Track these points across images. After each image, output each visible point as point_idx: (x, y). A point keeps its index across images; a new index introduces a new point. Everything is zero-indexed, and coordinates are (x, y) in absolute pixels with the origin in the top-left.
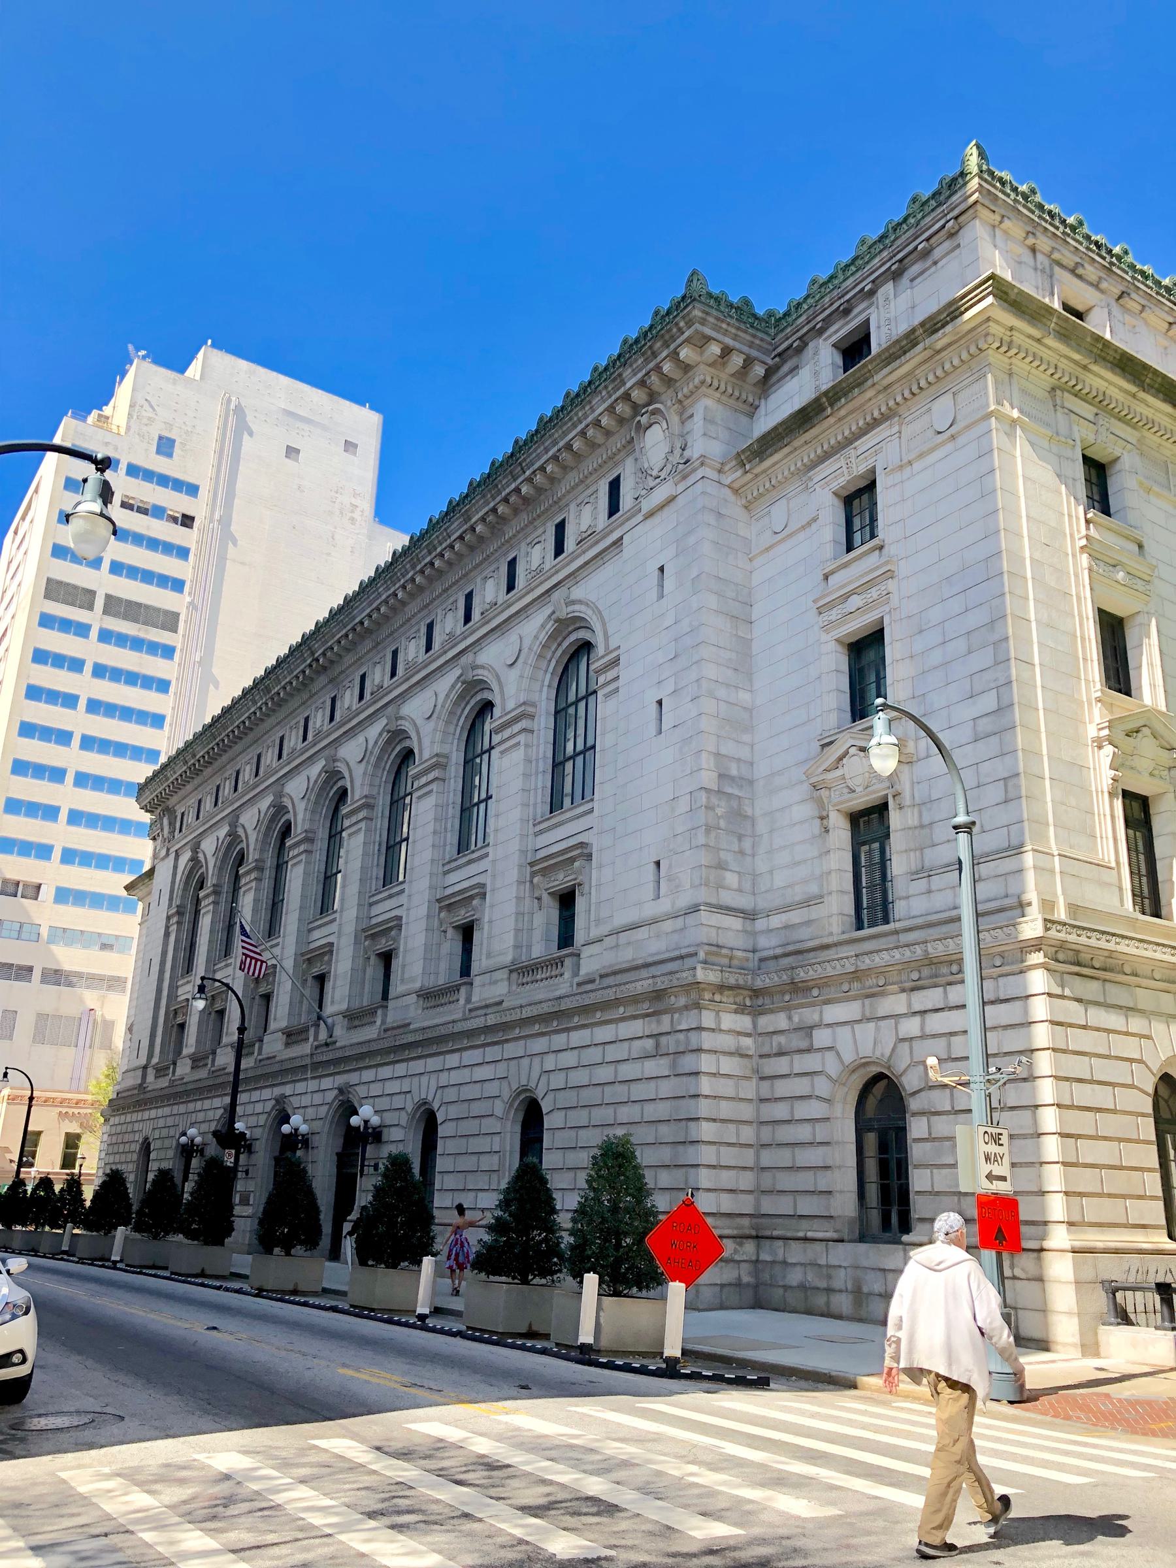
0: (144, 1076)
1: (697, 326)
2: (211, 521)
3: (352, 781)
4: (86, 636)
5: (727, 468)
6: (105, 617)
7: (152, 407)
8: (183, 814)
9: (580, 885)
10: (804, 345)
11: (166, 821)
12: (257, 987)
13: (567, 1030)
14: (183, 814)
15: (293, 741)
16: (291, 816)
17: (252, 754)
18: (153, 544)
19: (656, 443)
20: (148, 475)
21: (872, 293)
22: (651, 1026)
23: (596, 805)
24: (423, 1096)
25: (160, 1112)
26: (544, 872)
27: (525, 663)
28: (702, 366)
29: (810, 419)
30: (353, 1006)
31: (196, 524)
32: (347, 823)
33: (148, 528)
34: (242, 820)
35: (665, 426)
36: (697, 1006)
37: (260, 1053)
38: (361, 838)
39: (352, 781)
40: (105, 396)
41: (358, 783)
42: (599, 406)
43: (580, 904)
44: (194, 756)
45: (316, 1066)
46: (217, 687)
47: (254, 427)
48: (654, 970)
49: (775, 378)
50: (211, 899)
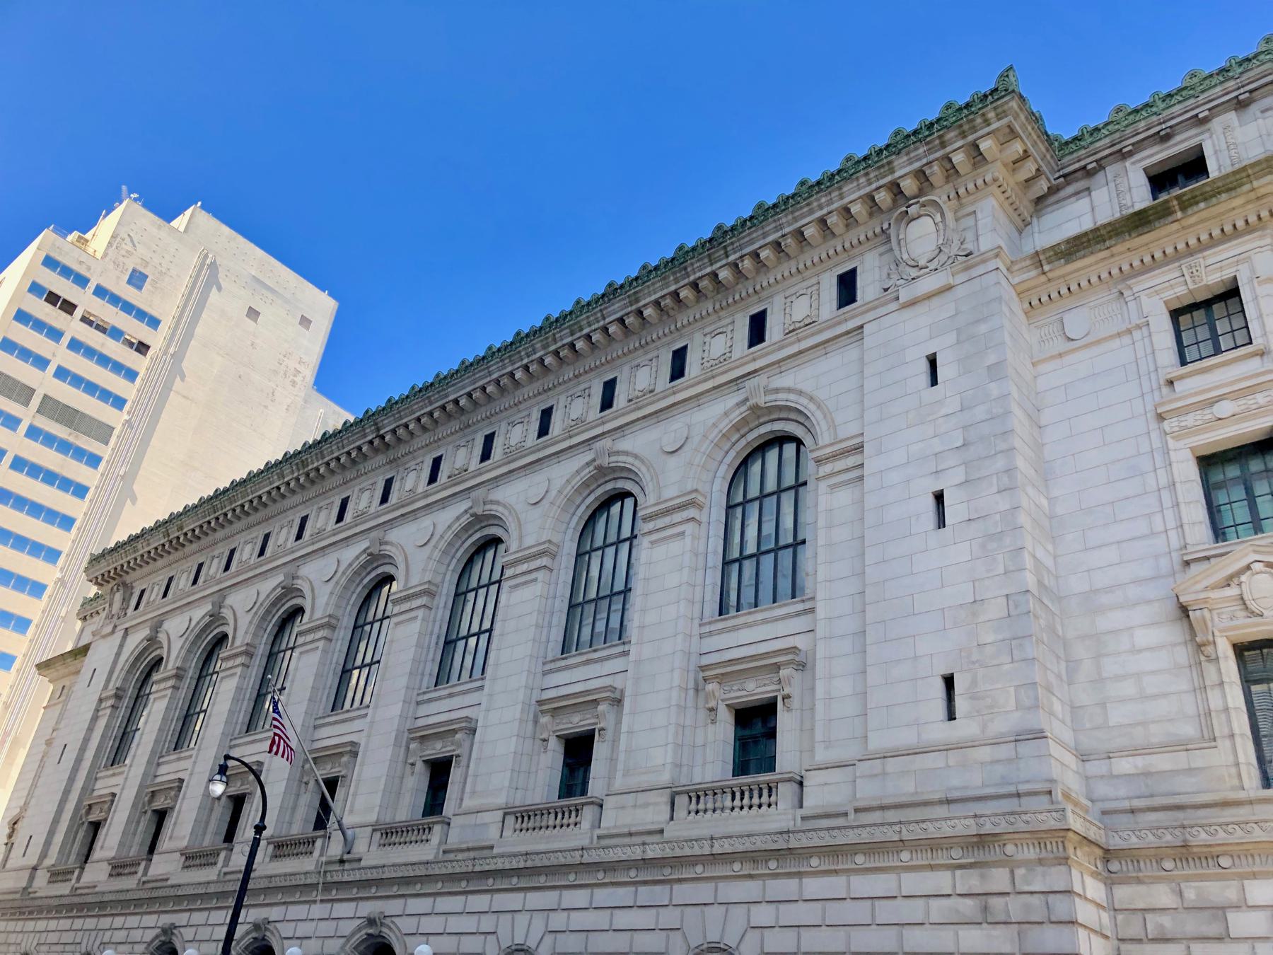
0: (32, 878)
1: (1010, 118)
2: (165, 353)
3: (235, 630)
4: (14, 430)
5: (1016, 267)
6: (38, 415)
7: (132, 241)
8: (143, 592)
9: (458, 756)
10: (1100, 167)
11: (118, 597)
12: (150, 802)
13: (799, 875)
14: (143, 592)
15: (247, 553)
16: (229, 630)
17: (259, 534)
18: (104, 360)
19: (921, 236)
20: (115, 300)
21: (1205, 121)
22: (971, 881)
23: (487, 683)
24: (519, 940)
25: (53, 924)
26: (722, 678)
27: (435, 547)
28: (999, 164)
29: (1149, 222)
30: (382, 820)
31: (150, 353)
32: (155, 688)
33: (103, 345)
34: (166, 626)
35: (938, 218)
36: (1064, 861)
37: (145, 873)
38: (315, 658)
39: (235, 630)
40: (87, 224)
41: (240, 633)
42: (853, 194)
43: (455, 775)
44: (181, 528)
45: (328, 887)
46: (134, 503)
47: (223, 284)
48: (979, 808)
49: (1052, 199)
50: (171, 683)
